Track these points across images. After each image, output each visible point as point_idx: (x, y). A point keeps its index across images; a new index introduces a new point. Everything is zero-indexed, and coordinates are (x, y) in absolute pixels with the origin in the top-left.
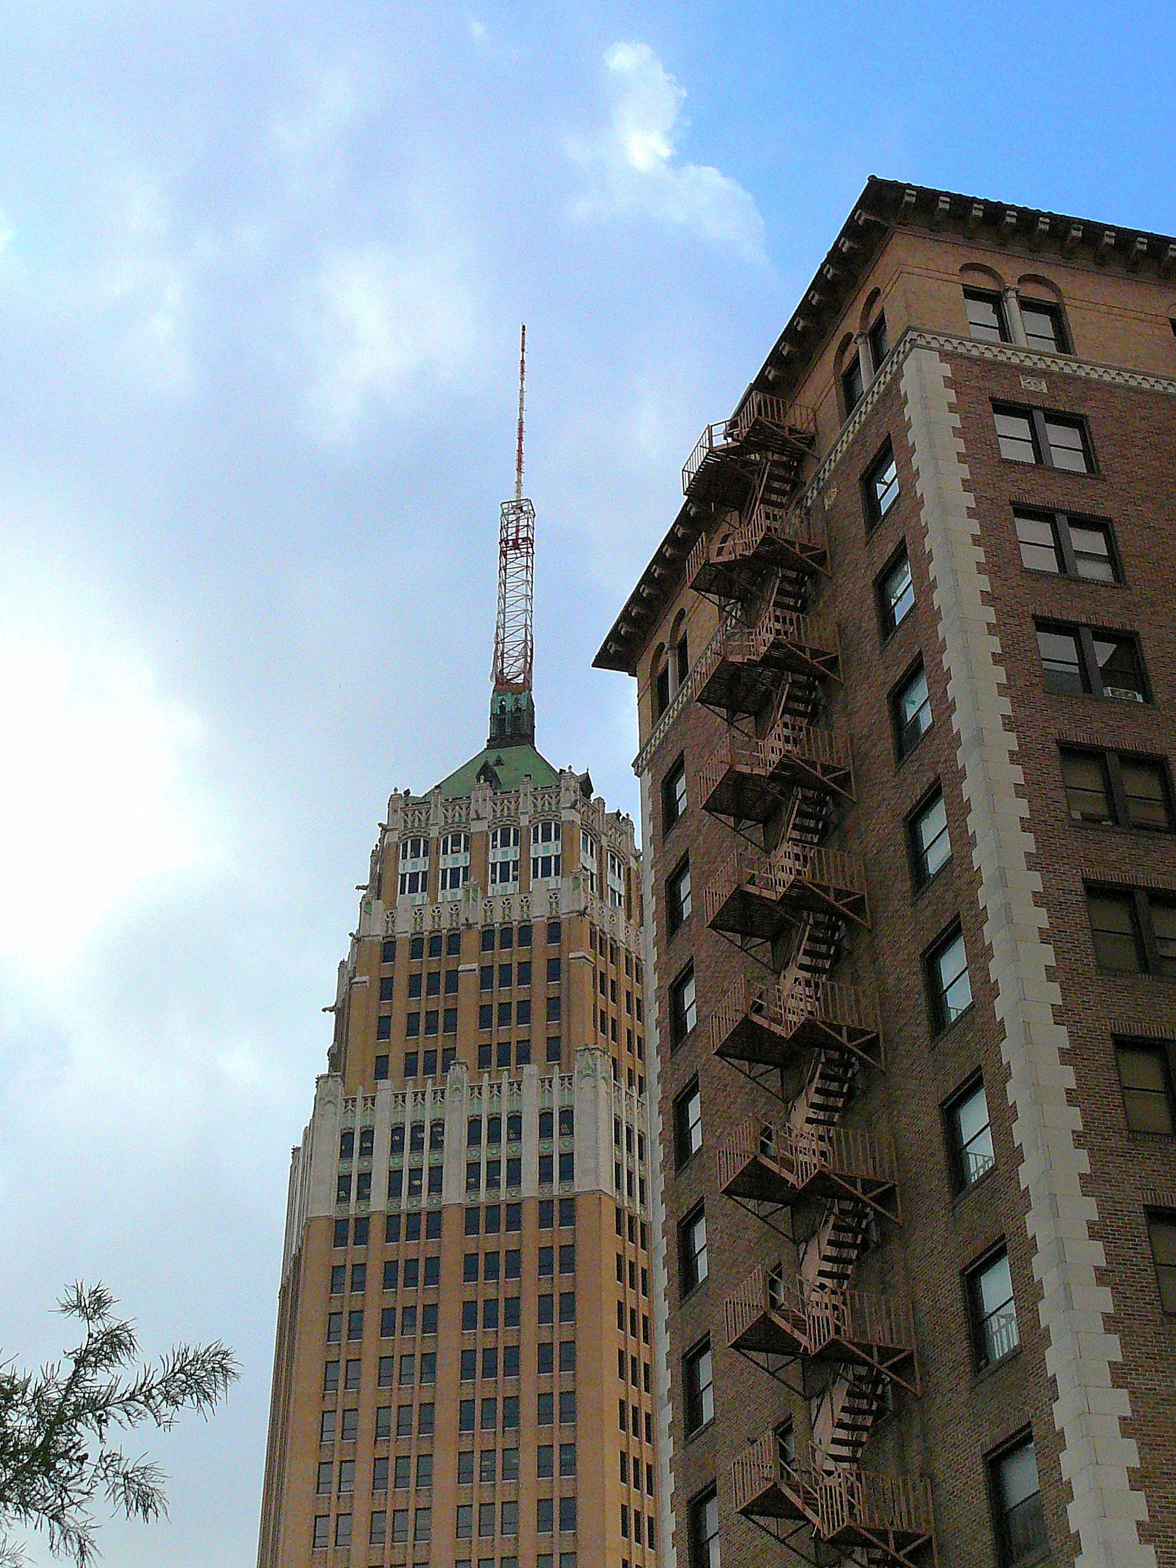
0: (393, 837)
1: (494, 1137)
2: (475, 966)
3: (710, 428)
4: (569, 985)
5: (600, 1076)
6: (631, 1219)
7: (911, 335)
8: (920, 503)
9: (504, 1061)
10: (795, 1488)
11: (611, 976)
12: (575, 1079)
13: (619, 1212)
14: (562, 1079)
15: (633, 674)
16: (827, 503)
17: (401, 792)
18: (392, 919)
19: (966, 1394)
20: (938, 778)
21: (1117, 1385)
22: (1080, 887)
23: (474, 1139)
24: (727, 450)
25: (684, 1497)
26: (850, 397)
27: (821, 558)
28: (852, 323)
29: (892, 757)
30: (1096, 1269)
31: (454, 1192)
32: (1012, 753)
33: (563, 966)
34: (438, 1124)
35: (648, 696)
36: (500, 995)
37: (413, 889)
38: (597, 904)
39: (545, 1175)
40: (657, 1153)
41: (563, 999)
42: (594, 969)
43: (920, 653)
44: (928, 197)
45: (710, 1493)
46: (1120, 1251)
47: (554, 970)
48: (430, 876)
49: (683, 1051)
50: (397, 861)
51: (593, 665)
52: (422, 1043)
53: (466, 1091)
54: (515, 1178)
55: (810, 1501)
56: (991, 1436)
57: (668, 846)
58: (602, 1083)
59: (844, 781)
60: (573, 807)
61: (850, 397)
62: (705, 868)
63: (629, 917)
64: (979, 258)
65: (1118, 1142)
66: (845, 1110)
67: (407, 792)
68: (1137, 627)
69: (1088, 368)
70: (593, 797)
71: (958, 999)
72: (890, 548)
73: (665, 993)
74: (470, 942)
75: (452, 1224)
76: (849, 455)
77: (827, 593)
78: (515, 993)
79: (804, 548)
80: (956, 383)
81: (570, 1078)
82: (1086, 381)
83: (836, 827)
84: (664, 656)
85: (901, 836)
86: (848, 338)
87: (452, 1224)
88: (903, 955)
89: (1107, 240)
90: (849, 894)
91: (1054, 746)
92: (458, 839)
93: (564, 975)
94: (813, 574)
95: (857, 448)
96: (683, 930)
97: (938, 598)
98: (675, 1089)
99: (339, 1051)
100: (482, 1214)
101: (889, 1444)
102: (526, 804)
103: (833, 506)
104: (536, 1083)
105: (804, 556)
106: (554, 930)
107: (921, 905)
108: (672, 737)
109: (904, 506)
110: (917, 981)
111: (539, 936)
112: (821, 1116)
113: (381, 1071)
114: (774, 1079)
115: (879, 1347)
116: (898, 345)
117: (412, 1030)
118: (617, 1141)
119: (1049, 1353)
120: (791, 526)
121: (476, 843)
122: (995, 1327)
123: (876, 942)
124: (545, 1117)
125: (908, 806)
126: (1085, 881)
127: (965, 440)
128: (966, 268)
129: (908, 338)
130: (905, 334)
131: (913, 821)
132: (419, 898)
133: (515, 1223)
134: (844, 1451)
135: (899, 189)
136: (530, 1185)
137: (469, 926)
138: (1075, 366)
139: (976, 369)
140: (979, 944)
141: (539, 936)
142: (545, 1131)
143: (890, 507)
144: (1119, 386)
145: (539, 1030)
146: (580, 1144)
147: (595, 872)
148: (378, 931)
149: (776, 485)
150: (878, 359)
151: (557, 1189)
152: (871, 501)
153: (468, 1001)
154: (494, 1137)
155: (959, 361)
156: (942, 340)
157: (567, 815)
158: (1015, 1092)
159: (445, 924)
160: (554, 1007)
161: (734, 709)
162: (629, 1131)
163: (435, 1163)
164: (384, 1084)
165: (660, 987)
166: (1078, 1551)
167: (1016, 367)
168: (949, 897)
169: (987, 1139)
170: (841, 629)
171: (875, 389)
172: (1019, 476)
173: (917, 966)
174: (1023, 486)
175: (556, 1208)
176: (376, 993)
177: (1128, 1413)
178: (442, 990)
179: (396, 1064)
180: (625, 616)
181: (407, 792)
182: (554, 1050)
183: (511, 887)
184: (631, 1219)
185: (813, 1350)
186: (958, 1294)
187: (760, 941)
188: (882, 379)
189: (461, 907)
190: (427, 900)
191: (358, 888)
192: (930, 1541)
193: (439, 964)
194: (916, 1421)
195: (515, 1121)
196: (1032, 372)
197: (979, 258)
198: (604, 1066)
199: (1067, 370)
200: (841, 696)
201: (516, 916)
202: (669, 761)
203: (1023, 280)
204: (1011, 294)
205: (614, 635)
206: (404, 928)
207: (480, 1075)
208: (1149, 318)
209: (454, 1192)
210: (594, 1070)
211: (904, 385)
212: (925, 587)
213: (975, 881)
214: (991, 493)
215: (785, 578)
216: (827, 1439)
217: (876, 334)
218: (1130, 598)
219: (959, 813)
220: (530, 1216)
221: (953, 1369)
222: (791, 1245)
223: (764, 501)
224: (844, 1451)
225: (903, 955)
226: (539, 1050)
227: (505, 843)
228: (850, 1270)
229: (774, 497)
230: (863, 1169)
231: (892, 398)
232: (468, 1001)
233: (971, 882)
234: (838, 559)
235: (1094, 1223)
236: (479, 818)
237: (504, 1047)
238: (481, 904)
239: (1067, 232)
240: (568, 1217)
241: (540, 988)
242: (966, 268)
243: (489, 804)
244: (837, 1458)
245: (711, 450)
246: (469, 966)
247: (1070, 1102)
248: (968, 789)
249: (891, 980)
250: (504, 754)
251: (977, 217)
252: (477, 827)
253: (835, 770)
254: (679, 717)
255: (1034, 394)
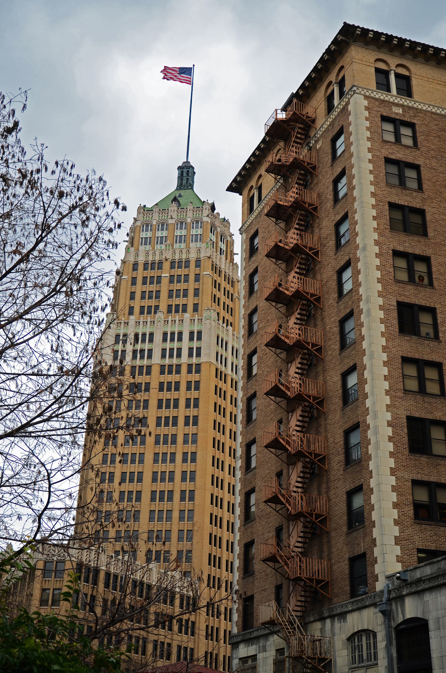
0: (139, 223)
1: (172, 340)
2: (168, 275)
3: (276, 110)
4: (203, 284)
5: (212, 319)
6: (221, 372)
7: (355, 88)
8: (352, 155)
9: (177, 311)
10: (283, 496)
11: (218, 281)
12: (203, 320)
13: (217, 370)
14: (199, 319)
15: (241, 194)
16: (318, 146)
17: (142, 206)
18: (137, 255)
19: (342, 472)
20: (350, 259)
21: (392, 475)
22: (395, 304)
23: (165, 340)
24: (282, 121)
25: (244, 492)
26: (330, 107)
27: (314, 168)
28: (332, 77)
29: (334, 248)
30: (389, 436)
31: (156, 359)
32: (376, 254)
33: (201, 277)
34: (152, 335)
35: (246, 205)
36: (176, 286)
37: (146, 244)
38: (215, 254)
39: (190, 355)
40: (241, 373)
41: (201, 289)
42: (213, 279)
43: (347, 212)
44: (365, 31)
45: (253, 491)
46: (397, 431)
47: (197, 278)
48: (153, 238)
49: (252, 339)
50: (140, 233)
51: (227, 190)
52: (146, 303)
53: (162, 322)
54: (179, 355)
55: (288, 501)
56: (349, 486)
57: (250, 263)
58: (213, 322)
59: (316, 253)
60: (208, 216)
61: (330, 107)
62: (264, 274)
63: (226, 259)
64: (382, 56)
65: (400, 394)
66: (308, 370)
67: (145, 206)
68: (425, 207)
69: (417, 104)
70: (215, 212)
71: (347, 287)
72: (340, 170)
73: (247, 316)
74: (166, 265)
75: (155, 370)
76: (327, 130)
77: (315, 181)
78: (182, 286)
79: (308, 164)
80: (369, 109)
81: (201, 320)
82: (417, 109)
83: (312, 269)
84: (252, 191)
85: (335, 277)
86: (331, 83)
87: (155, 370)
88: (332, 319)
89: (430, 52)
90: (315, 295)
91: (391, 252)
92: (163, 225)
93: (201, 280)
94: (311, 173)
95: (330, 128)
96: (255, 295)
97: (353, 149)
98: (248, 351)
99: (115, 303)
100: (167, 367)
101: (315, 484)
102: (190, 214)
103: (320, 148)
104: (189, 320)
105: (308, 167)
106: (198, 263)
107: (341, 303)
108: (254, 221)
109: (346, 154)
110: (336, 330)
111: (192, 265)
112: (300, 371)
113: (131, 311)
114: (283, 355)
115: (315, 454)
116: (349, 91)
117: (143, 298)
118: (218, 344)
119: (371, 463)
120: (304, 154)
121: (171, 227)
122: (350, 393)
123: (324, 313)
124: (192, 333)
125: (338, 267)
126: (398, 302)
127: (370, 132)
128: (377, 60)
129: (353, 89)
130: (352, 88)
131: (340, 272)
132: (148, 247)
133: (178, 372)
134: (300, 485)
135: (354, 27)
136: (185, 359)
137: (166, 260)
138: (413, 103)
139: (377, 103)
140: (359, 321)
141: (192, 265)
142: (191, 339)
143: (341, 154)
144: (429, 111)
145: (190, 301)
146: (203, 344)
147: (215, 241)
148: (132, 259)
149: (299, 136)
150: (342, 94)
151: (194, 360)
152: (334, 150)
153: (165, 287)
154: (172, 340)
155: (371, 100)
156: (365, 91)
157: (205, 219)
158: (366, 374)
159: (157, 258)
160: (197, 292)
161: (277, 218)
162: (222, 340)
163: (150, 348)
164: (132, 317)
165: (245, 314)
166: (374, 526)
167: (392, 103)
168: (350, 303)
169: (350, 282)
170: (319, 196)
171: (339, 106)
172: (388, 147)
173: (337, 324)
174: (390, 151)
175: (194, 367)
176: (130, 283)
177: (394, 484)
178: (155, 283)
179: (137, 310)
180: (239, 174)
181: (145, 206)
182: (196, 308)
183: (183, 245)
184: (221, 372)
185: (293, 452)
186: (342, 439)
187: (282, 305)
188: (342, 103)
189: (164, 252)
190: (151, 248)
191: (124, 241)
192: (326, 517)
193: (155, 273)
194: (325, 478)
195: (180, 334)
196: (397, 105)
197: (382, 56)
198: (214, 315)
199: (410, 105)
200: (317, 221)
201: (184, 257)
202: (252, 232)
203: (398, 66)
204: (392, 72)
205: (235, 180)
206: (141, 259)
207: (168, 316)
208: (443, 83)
209: (156, 359)
210: (211, 317)
211: (350, 108)
212: (348, 145)
213: (360, 299)
214: (378, 154)
215: (300, 174)
216: (294, 480)
217: (341, 83)
218: (423, 196)
219: (357, 272)
220: (184, 369)
221: (338, 463)
222: (286, 413)
223: (295, 142)
224: (300, 485)
225: (332, 319)
226: (190, 308)
227: (181, 228)
228: (306, 425)
229: (298, 140)
230: (313, 392)
231: (345, 111)
232: (165, 287)
233: (358, 299)
234: (320, 169)
235: (390, 421)
236: (172, 218)
237: (177, 306)
238: (171, 251)
239: (416, 48)
240: (198, 371)
241: (191, 285)
242: (377, 60)
243: (176, 212)
244: (297, 487)
245: (276, 119)
246: (165, 275)
247: (385, 379)
248: (360, 265)
249: (328, 327)
250: (182, 192)
251: (383, 41)
252: (171, 221)
253: (314, 249)
254: (257, 215)
255: (397, 114)
